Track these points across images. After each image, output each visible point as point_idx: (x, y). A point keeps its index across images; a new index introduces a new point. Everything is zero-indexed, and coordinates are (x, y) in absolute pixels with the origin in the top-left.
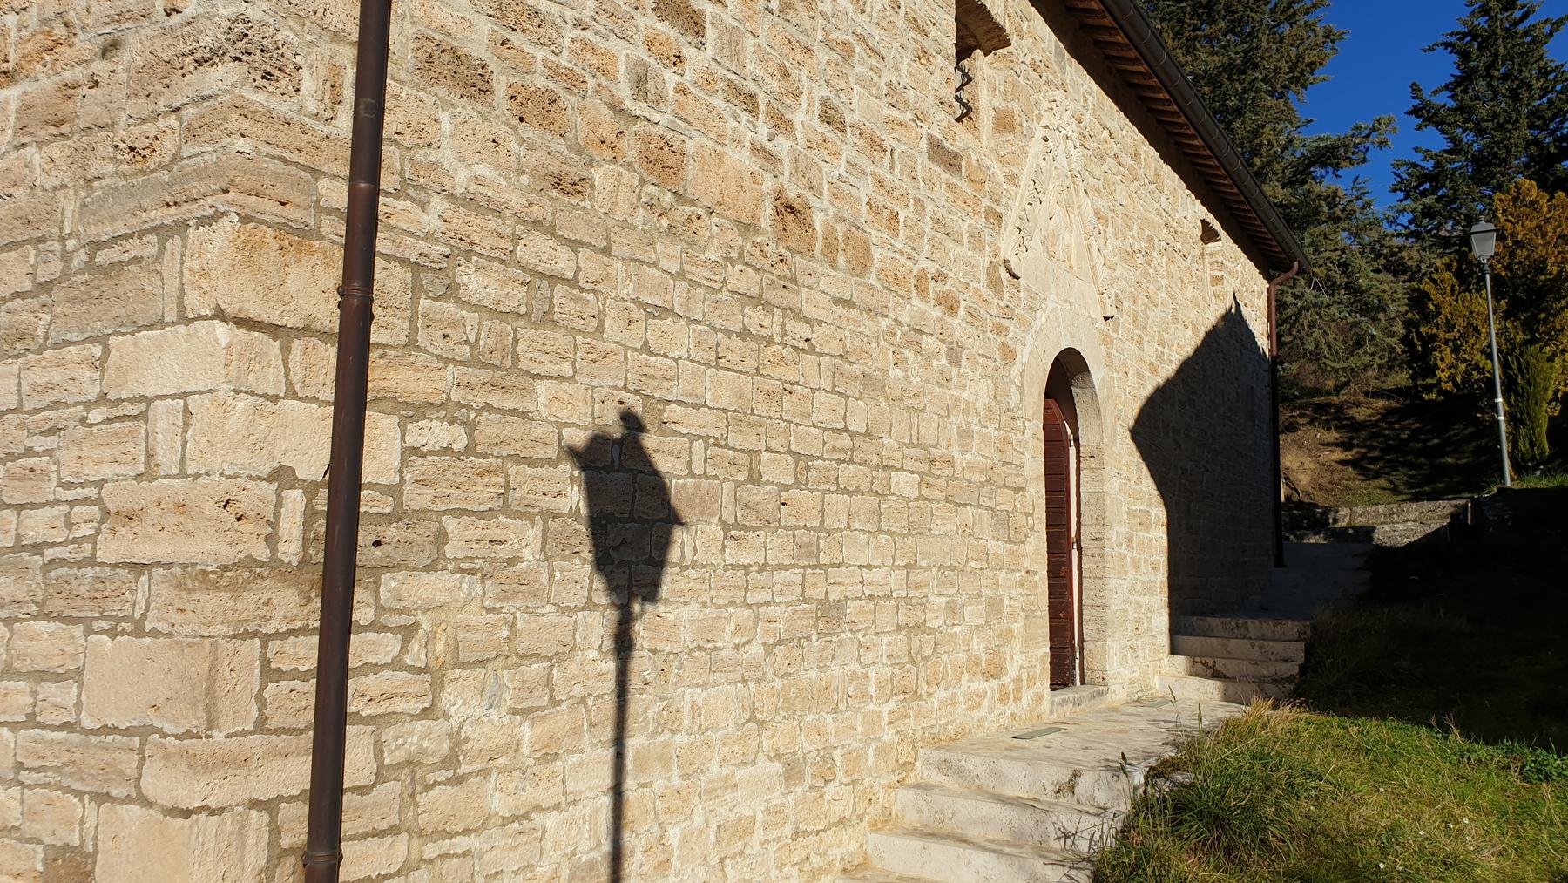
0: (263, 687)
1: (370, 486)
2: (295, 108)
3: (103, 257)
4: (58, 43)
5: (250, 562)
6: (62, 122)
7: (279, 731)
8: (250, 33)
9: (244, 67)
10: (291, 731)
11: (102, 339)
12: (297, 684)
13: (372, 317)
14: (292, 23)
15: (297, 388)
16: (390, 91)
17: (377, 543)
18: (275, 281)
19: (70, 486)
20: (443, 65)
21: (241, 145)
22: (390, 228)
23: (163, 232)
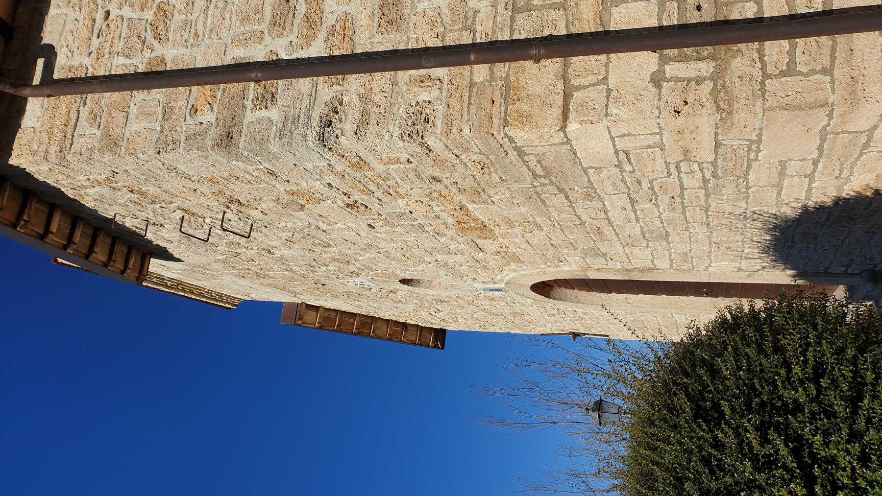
0: (800, 73)
1: (660, 20)
2: (439, 102)
3: (539, 171)
4: (440, 195)
5: (714, 93)
6: (477, 191)
7: (833, 58)
8: (407, 133)
9: (425, 134)
10: (834, 50)
11: (585, 170)
12: (799, 50)
13: (550, 35)
14: (395, 110)
15: (600, 77)
16: (415, 46)
17: (699, 8)
18: (538, 101)
19: (669, 174)
20: (391, 14)
21: (466, 130)
22: (494, 32)
23: (521, 153)
